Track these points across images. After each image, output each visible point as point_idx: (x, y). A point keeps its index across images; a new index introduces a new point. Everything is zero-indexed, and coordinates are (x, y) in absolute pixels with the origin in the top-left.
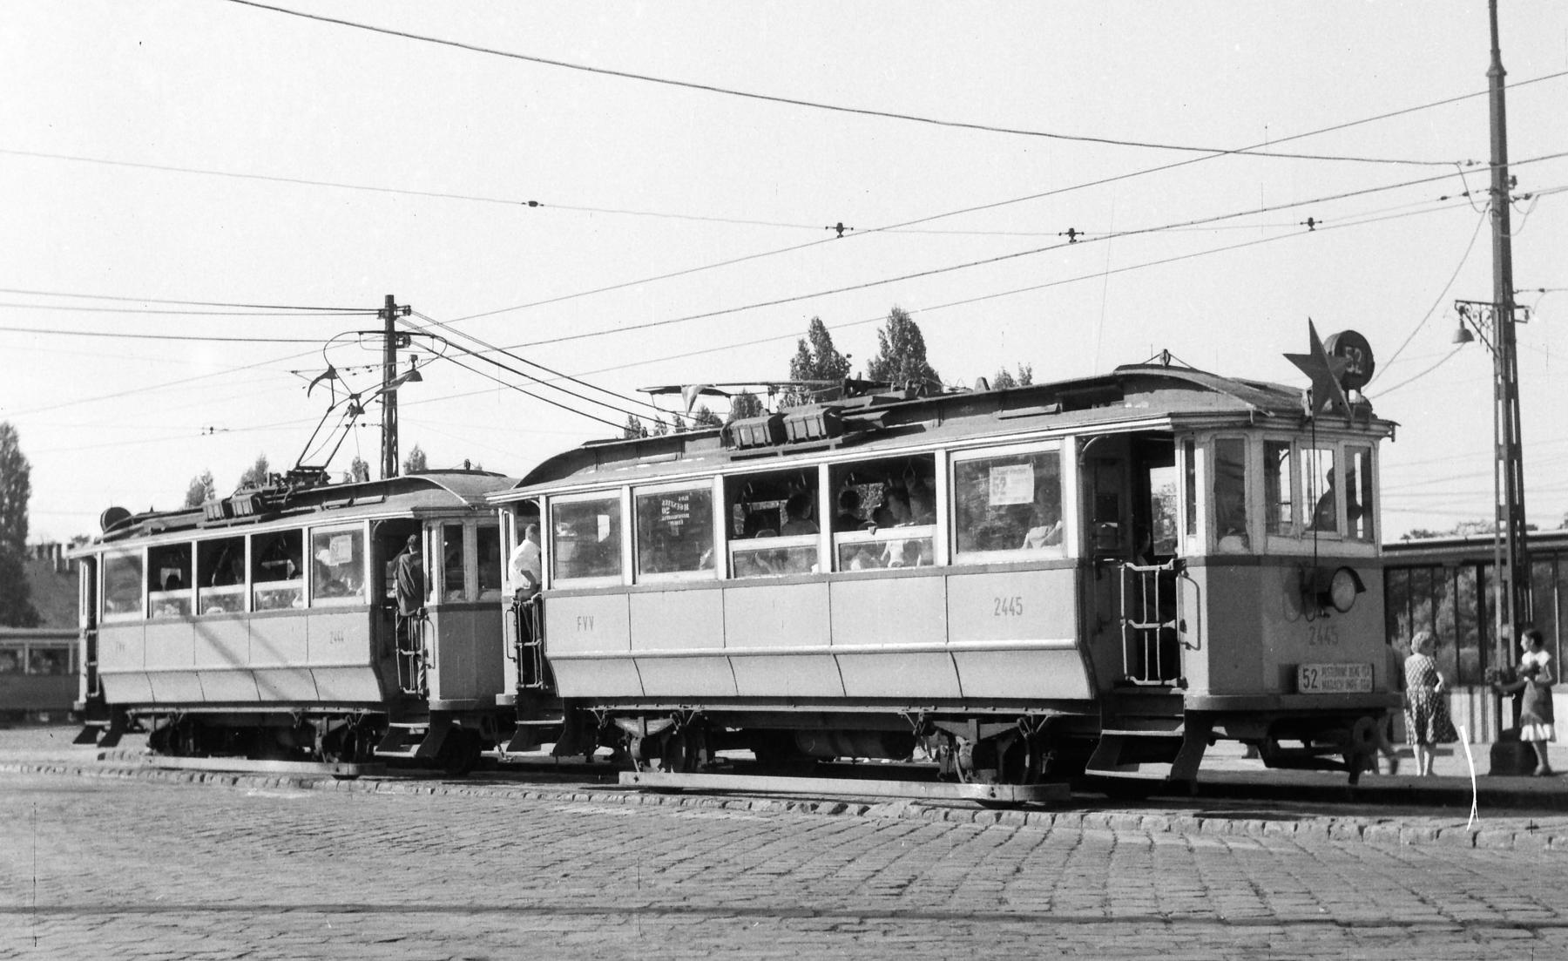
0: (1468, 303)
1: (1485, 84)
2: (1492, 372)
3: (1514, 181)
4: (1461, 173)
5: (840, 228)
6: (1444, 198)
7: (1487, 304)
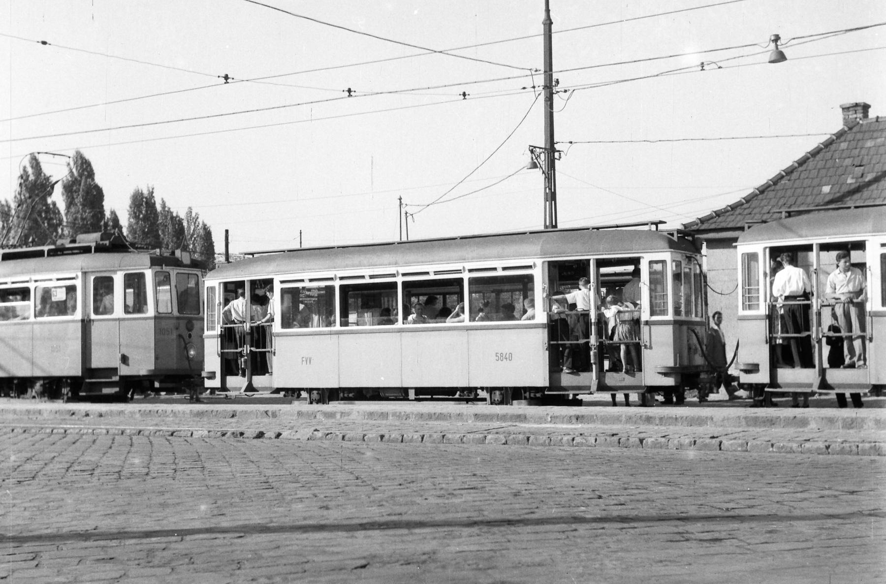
0: (535, 147)
1: (541, 29)
2: (543, 187)
3: (557, 82)
4: (532, 75)
5: (226, 77)
6: (524, 88)
7: (540, 148)
